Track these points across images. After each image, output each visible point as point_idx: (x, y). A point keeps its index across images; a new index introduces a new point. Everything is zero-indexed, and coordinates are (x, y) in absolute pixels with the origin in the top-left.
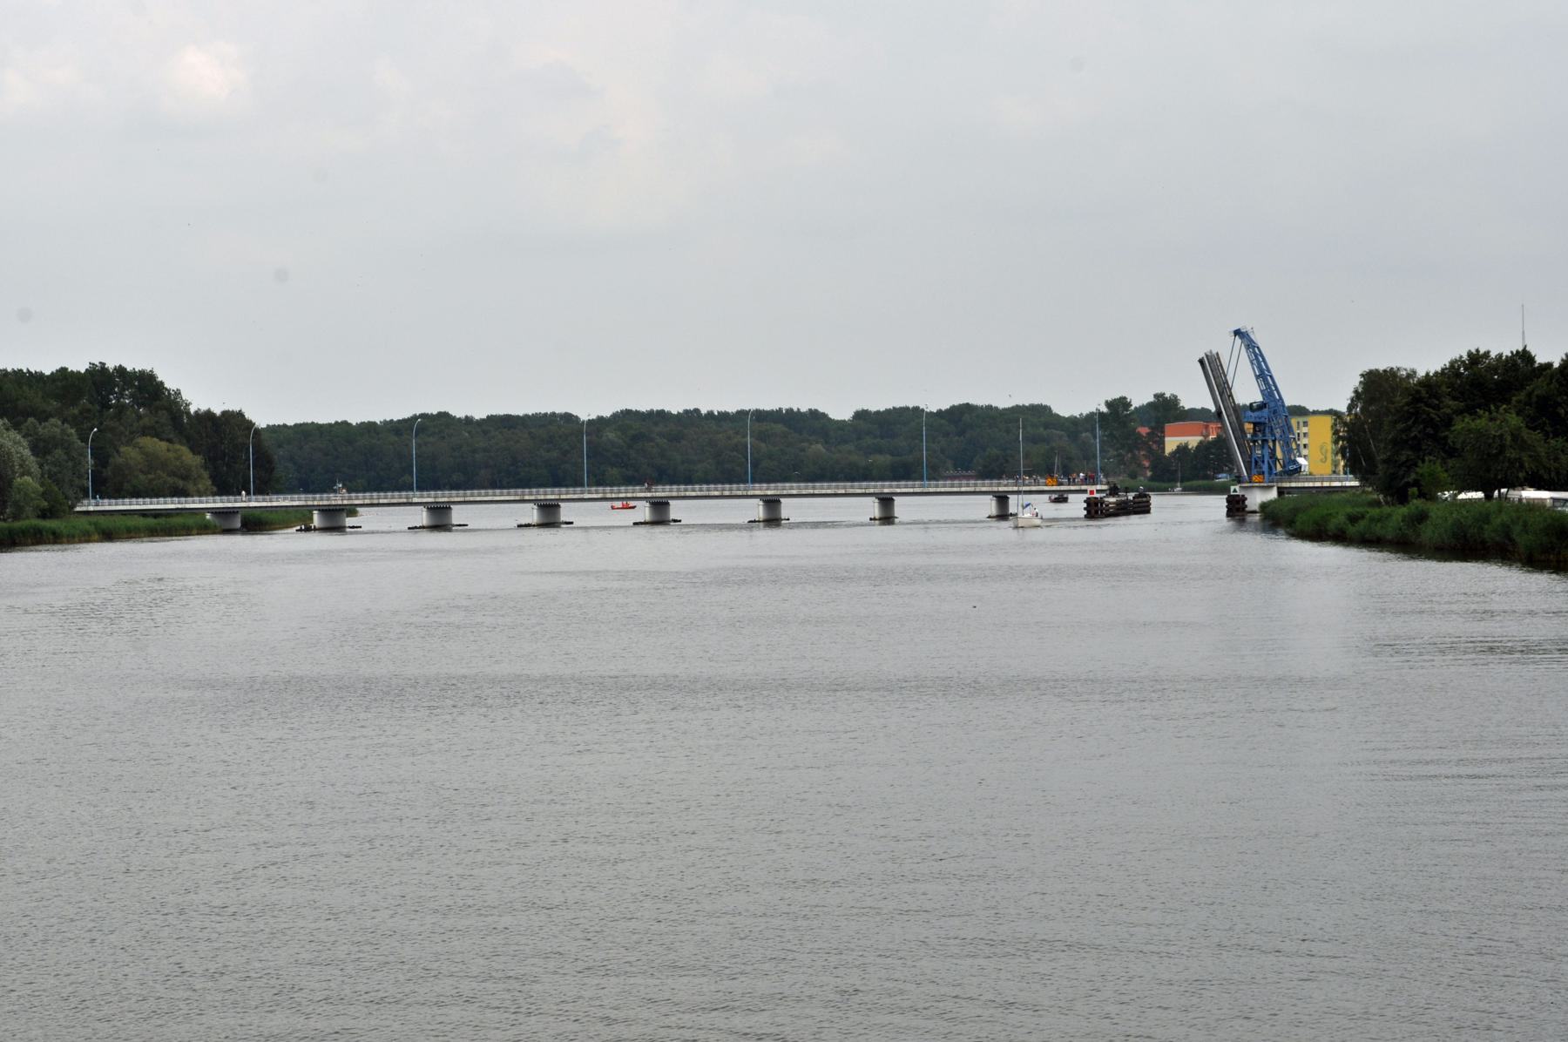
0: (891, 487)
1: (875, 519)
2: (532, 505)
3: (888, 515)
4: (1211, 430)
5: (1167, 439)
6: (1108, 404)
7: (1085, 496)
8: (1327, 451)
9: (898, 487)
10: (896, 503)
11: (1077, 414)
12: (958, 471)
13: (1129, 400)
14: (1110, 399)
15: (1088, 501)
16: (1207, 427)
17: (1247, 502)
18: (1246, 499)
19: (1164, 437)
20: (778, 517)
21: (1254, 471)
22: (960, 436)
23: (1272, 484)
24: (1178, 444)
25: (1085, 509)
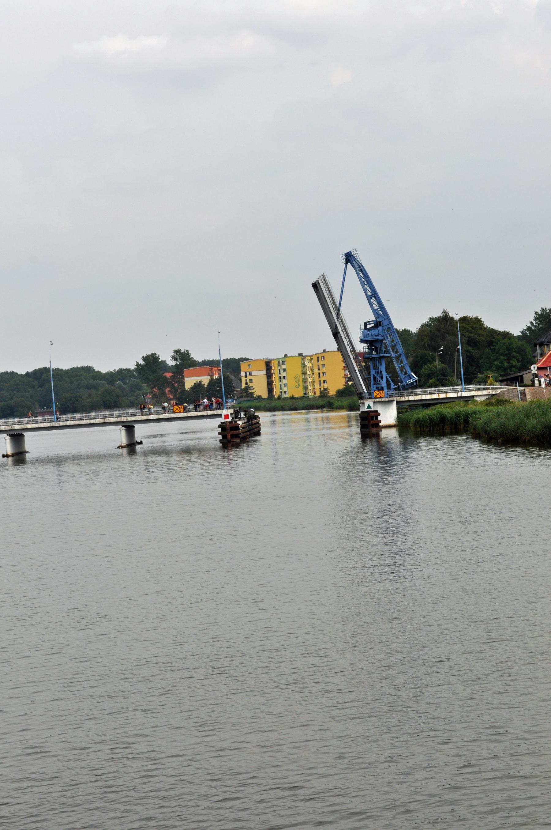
0: (21, 423)
1: (7, 456)
2: (5, 435)
3: (20, 451)
4: (214, 372)
5: (186, 379)
6: (144, 359)
7: (219, 421)
8: (299, 381)
9: (29, 422)
10: (26, 439)
11: (112, 370)
12: (44, 409)
13: (157, 356)
14: (145, 355)
15: (223, 426)
16: (212, 370)
17: (380, 418)
18: (379, 414)
19: (183, 377)
20: (24, 450)
21: (374, 387)
22: (41, 387)
23: (391, 399)
24: (195, 381)
25: (220, 434)
